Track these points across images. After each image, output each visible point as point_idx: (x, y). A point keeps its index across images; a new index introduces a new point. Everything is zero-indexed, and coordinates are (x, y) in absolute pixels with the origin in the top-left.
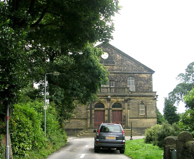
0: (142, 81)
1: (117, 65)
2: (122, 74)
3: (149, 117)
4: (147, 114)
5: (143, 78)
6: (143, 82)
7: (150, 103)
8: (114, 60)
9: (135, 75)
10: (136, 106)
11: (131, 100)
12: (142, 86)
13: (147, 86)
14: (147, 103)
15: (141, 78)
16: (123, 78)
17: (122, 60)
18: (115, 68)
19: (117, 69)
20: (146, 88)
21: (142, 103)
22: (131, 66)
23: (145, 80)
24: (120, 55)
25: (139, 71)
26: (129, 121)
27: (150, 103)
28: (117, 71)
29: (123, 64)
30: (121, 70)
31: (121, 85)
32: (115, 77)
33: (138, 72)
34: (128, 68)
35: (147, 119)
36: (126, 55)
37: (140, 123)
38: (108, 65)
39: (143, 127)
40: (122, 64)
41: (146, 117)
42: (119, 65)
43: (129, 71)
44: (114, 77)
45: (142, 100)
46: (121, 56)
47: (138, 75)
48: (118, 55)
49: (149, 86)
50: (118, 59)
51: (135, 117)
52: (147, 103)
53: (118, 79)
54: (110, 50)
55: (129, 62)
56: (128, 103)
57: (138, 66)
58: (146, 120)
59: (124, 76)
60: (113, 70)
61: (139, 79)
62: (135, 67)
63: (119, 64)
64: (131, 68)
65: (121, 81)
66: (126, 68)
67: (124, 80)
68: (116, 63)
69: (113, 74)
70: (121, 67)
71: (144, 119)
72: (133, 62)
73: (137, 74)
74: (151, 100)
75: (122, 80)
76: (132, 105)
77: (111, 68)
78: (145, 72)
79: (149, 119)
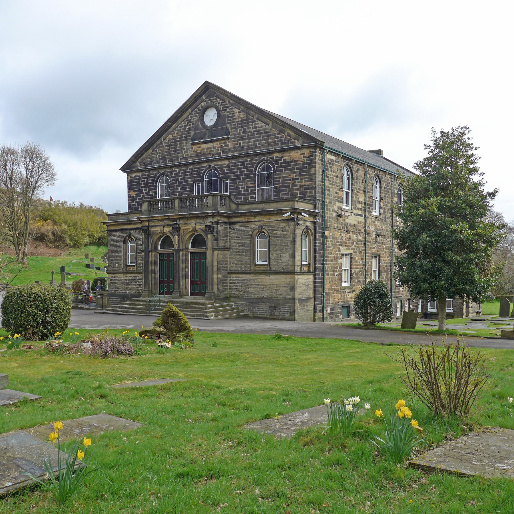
0: (290, 169)
1: (234, 138)
2: (245, 159)
3: (276, 269)
4: (273, 262)
5: (291, 162)
6: (293, 173)
7: (279, 232)
8: (228, 126)
9: (274, 155)
10: (246, 240)
11: (237, 227)
12: (289, 186)
13: (303, 183)
14: (273, 230)
15: (287, 162)
16: (246, 168)
17: (246, 121)
18: (231, 145)
19: (234, 148)
20: (298, 189)
21: (261, 233)
22: (265, 133)
23: (297, 169)
24: (242, 108)
25: (282, 144)
26: (215, 281)
27: (279, 232)
28: (234, 151)
29: (248, 130)
30: (241, 148)
31: (242, 188)
32: (231, 169)
33: (280, 146)
34: (257, 141)
35: (272, 277)
36: (147, 144)
37: (254, 285)
38: (215, 141)
39: (261, 296)
40: (245, 132)
41: (269, 272)
42: (238, 137)
43: (260, 147)
44: (227, 170)
45: (259, 224)
46: (242, 111)
47: (280, 155)
48: (236, 111)
49: (306, 183)
50: (237, 120)
51: (243, 268)
52: (273, 230)
53: (237, 172)
54: (221, 99)
55: (260, 124)
56: (215, 234)
57: (281, 131)
58: (268, 278)
59: (249, 164)
60: (226, 152)
61: (284, 167)
62: (275, 134)
63: (239, 134)
64: (265, 140)
65: (243, 178)
66: (255, 141)
67: (248, 174)
68: (232, 132)
69: (227, 162)
70: (242, 140)
71: (263, 276)
72: (268, 121)
73: (278, 154)
74: (283, 224)
75: (245, 174)
76: (239, 238)
77: (222, 146)
78: (297, 144)
79: (277, 277)
